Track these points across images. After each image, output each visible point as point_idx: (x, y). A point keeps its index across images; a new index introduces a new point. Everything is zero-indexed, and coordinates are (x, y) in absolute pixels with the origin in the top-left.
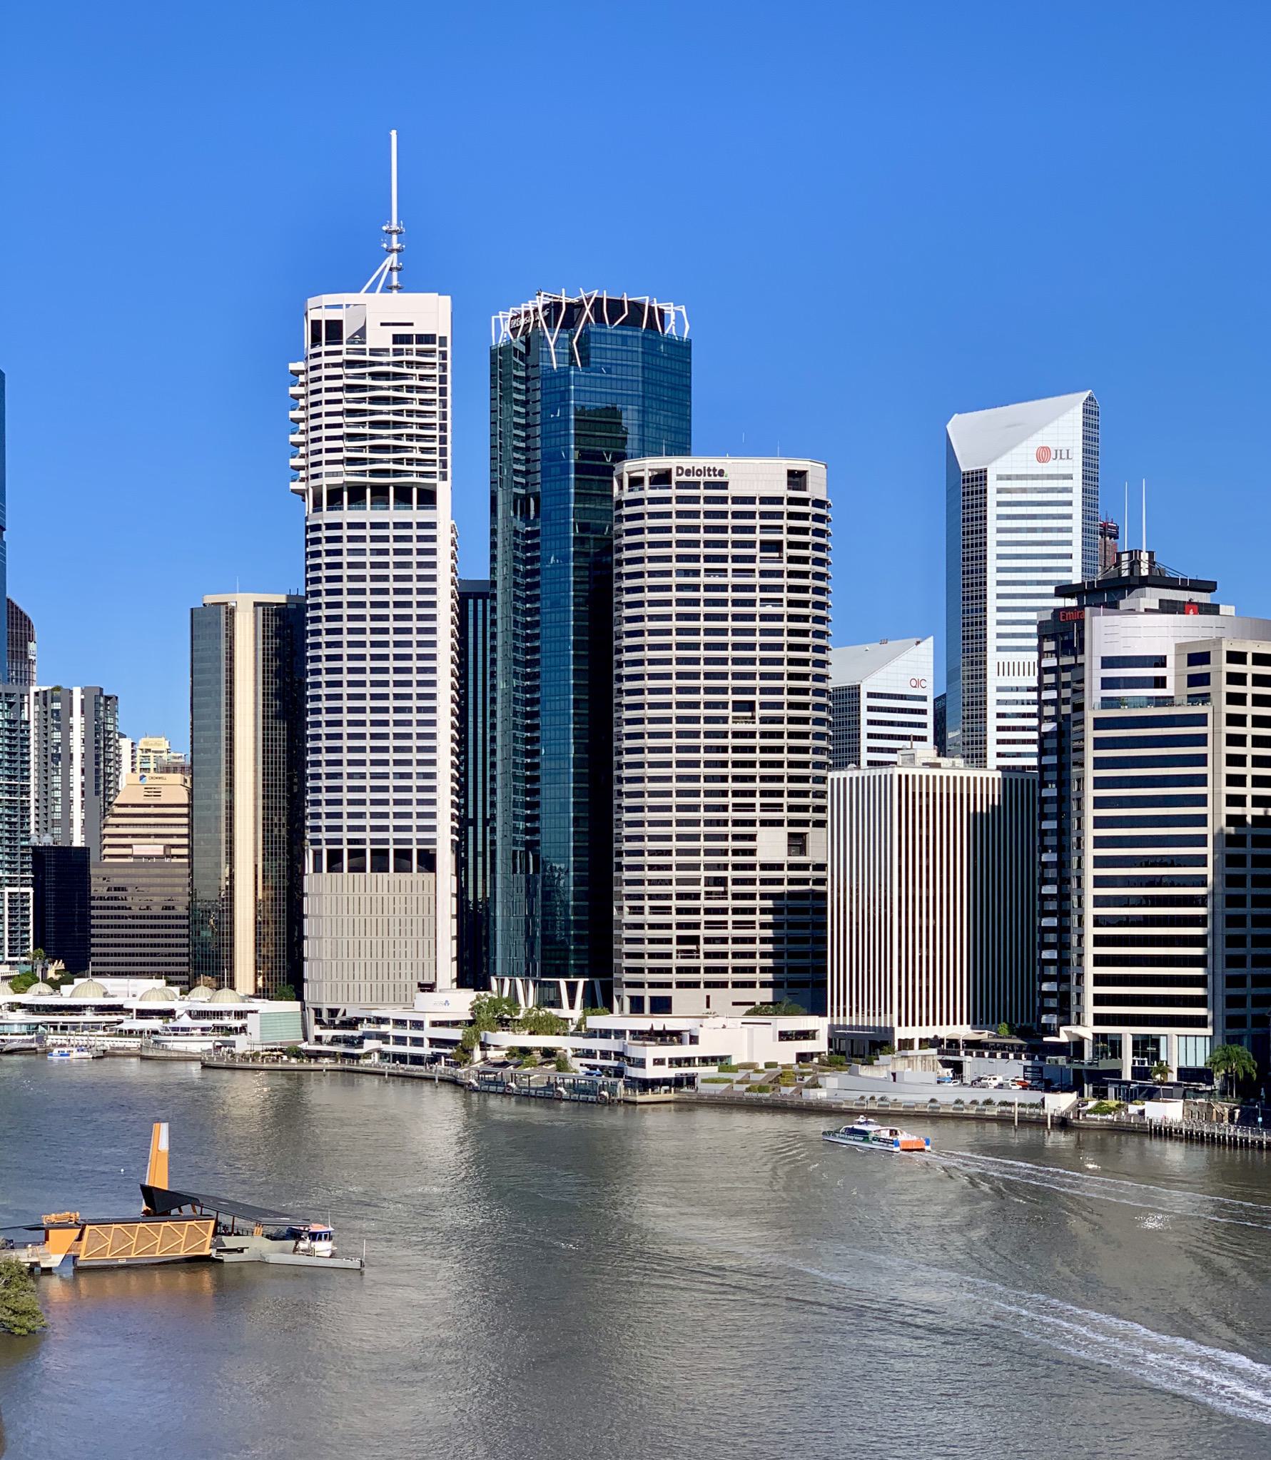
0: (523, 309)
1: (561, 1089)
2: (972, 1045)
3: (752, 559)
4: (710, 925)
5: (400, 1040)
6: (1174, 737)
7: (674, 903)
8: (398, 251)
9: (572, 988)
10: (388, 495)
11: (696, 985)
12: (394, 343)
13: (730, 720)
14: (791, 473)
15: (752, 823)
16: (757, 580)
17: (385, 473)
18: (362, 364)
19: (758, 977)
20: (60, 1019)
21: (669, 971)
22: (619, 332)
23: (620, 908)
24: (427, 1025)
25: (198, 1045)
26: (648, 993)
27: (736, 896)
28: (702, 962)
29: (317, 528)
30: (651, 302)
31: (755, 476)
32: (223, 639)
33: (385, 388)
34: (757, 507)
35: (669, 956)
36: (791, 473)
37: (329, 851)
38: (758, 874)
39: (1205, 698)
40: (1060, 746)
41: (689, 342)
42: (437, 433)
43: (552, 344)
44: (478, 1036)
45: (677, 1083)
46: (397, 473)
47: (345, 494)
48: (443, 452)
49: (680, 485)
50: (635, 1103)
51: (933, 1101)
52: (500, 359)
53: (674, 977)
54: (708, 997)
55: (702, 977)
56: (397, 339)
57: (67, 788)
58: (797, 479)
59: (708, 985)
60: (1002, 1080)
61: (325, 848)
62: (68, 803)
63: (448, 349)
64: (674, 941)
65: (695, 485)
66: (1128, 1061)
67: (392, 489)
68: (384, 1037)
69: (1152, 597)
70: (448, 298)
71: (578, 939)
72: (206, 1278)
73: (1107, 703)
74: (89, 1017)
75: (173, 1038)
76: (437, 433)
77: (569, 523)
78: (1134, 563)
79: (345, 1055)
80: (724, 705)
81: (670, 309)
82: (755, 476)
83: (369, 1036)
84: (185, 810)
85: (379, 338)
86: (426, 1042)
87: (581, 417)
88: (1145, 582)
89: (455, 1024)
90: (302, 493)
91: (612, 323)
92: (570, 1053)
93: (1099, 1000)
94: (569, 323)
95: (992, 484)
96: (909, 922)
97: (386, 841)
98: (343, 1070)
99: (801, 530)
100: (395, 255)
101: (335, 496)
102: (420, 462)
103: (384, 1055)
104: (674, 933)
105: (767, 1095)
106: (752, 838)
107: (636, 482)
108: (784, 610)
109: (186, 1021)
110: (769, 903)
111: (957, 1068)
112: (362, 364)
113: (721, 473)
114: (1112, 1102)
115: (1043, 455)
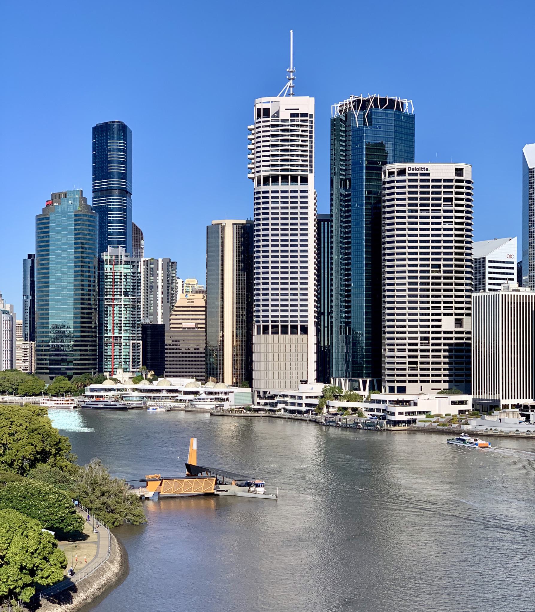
0: (344, 103)
1: (360, 425)
3: (440, 205)
4: (422, 357)
5: (293, 404)
8: (293, 79)
9: (364, 382)
10: (288, 179)
11: (416, 381)
12: (291, 117)
13: (431, 272)
14: (457, 169)
15: (440, 314)
16: (442, 214)
17: (287, 170)
18: (278, 126)
20: (152, 395)
21: (405, 375)
22: (384, 111)
23: (385, 350)
24: (304, 398)
25: (209, 406)
26: (396, 385)
27: (433, 345)
28: (419, 372)
29: (259, 193)
30: (398, 99)
31: (442, 170)
32: (220, 238)
33: (287, 135)
34: (442, 184)
35: (405, 369)
36: (457, 169)
37: (263, 325)
42: (308, 154)
43: (356, 117)
44: (325, 402)
46: (292, 170)
47: (270, 179)
48: (311, 161)
49: (410, 175)
50: (391, 430)
51: (517, 431)
52: (335, 123)
53: (407, 378)
54: (421, 387)
55: (419, 378)
56: (292, 115)
57: (156, 300)
58: (459, 172)
59: (421, 381)
61: (262, 324)
62: (156, 306)
63: (313, 119)
64: (407, 363)
65: (416, 175)
67: (289, 177)
68: (286, 403)
70: (313, 99)
71: (367, 362)
74: (164, 394)
75: (198, 403)
76: (308, 154)
77: (363, 191)
79: (270, 410)
80: (428, 266)
81: (406, 102)
82: (442, 170)
83: (280, 402)
84: (204, 309)
85: (285, 115)
86: (304, 405)
87: (368, 148)
89: (316, 397)
90: (253, 179)
91: (381, 108)
92: (364, 409)
94: (364, 108)
97: (287, 322)
98: (269, 417)
100: (291, 81)
101: (266, 180)
102: (301, 166)
103: (286, 410)
105: (446, 427)
106: (440, 320)
107: (391, 174)
108: (454, 226)
109: (203, 396)
110: (447, 348)
112: (278, 126)
113: (427, 169)
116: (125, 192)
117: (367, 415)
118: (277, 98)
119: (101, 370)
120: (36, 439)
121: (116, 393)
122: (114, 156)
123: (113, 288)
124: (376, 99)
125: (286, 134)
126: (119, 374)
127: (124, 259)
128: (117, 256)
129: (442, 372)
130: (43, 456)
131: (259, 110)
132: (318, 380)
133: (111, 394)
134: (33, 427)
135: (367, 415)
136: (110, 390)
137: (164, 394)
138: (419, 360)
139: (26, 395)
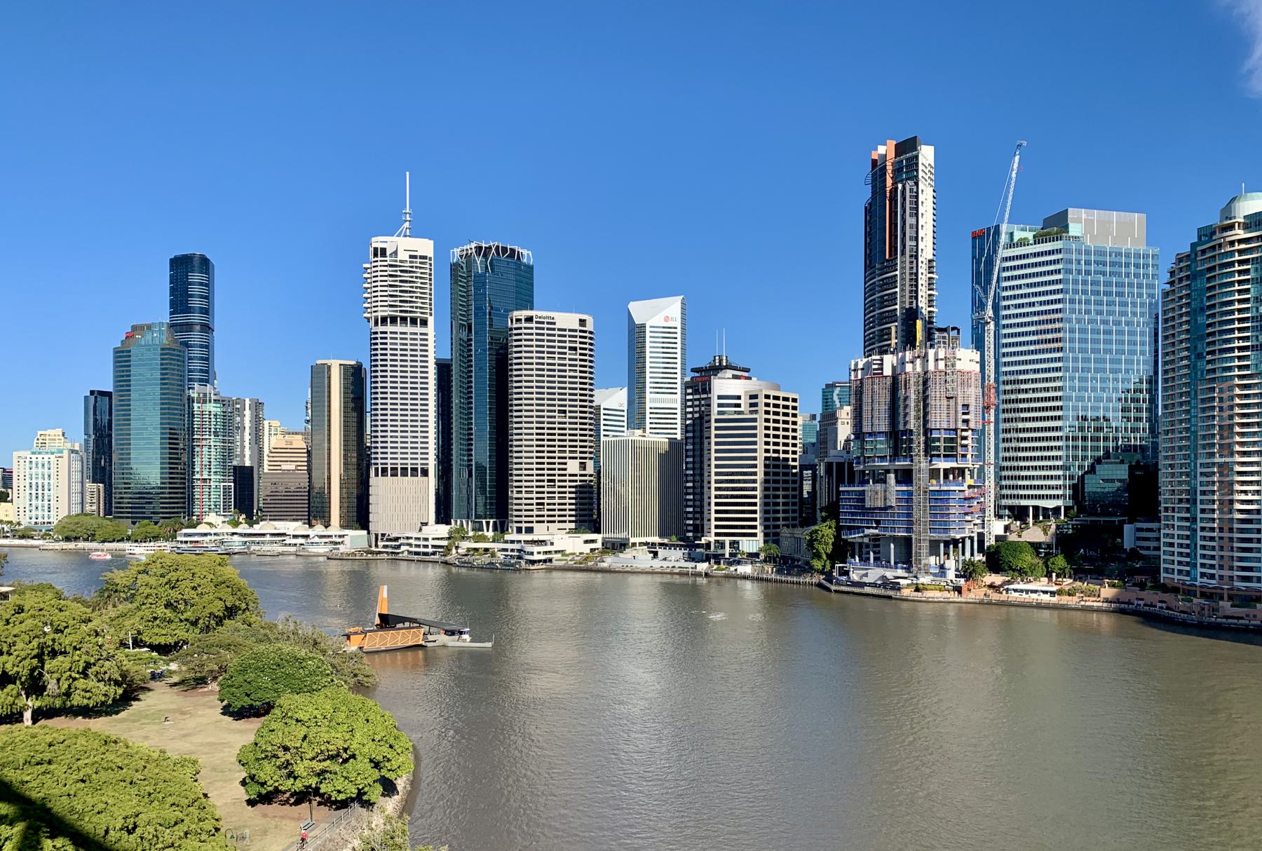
2: (661, 544)
5: (418, 546)
6: (748, 425)
7: (535, 489)
9: (488, 523)
16: (567, 362)
19: (568, 518)
20: (257, 539)
25: (322, 550)
26: (524, 525)
28: (546, 513)
33: (406, 277)
38: (568, 478)
39: (756, 412)
40: (697, 427)
45: (545, 561)
52: (455, 268)
53: (535, 519)
55: (546, 519)
57: (243, 441)
58: (582, 322)
60: (675, 558)
62: (243, 447)
66: (727, 551)
68: (410, 545)
69: (729, 373)
70: (432, 242)
71: (491, 504)
72: (421, 653)
73: (720, 413)
74: (268, 538)
78: (721, 361)
81: (525, 252)
82: (567, 320)
87: (488, 294)
88: (727, 367)
90: (368, 319)
93: (717, 527)
94: (485, 256)
95: (648, 329)
96: (634, 496)
99: (584, 342)
101: (384, 320)
103: (410, 552)
104: (535, 501)
107: (518, 320)
108: (578, 374)
109: (317, 539)
111: (655, 554)
114: (723, 566)
115: (666, 319)
116: (207, 328)
117: (501, 555)
118: (394, 238)
119: (191, 514)
120: (224, 592)
121: (213, 538)
122: (195, 290)
123: (202, 427)
124: (498, 247)
125: (401, 275)
126: (212, 518)
127: (213, 397)
128: (205, 395)
129: (568, 513)
130: (231, 612)
131: (376, 249)
132: (438, 522)
133: (207, 539)
134: (220, 579)
135: (501, 555)
136: (206, 535)
137: (268, 538)
138: (546, 501)
139: (103, 542)
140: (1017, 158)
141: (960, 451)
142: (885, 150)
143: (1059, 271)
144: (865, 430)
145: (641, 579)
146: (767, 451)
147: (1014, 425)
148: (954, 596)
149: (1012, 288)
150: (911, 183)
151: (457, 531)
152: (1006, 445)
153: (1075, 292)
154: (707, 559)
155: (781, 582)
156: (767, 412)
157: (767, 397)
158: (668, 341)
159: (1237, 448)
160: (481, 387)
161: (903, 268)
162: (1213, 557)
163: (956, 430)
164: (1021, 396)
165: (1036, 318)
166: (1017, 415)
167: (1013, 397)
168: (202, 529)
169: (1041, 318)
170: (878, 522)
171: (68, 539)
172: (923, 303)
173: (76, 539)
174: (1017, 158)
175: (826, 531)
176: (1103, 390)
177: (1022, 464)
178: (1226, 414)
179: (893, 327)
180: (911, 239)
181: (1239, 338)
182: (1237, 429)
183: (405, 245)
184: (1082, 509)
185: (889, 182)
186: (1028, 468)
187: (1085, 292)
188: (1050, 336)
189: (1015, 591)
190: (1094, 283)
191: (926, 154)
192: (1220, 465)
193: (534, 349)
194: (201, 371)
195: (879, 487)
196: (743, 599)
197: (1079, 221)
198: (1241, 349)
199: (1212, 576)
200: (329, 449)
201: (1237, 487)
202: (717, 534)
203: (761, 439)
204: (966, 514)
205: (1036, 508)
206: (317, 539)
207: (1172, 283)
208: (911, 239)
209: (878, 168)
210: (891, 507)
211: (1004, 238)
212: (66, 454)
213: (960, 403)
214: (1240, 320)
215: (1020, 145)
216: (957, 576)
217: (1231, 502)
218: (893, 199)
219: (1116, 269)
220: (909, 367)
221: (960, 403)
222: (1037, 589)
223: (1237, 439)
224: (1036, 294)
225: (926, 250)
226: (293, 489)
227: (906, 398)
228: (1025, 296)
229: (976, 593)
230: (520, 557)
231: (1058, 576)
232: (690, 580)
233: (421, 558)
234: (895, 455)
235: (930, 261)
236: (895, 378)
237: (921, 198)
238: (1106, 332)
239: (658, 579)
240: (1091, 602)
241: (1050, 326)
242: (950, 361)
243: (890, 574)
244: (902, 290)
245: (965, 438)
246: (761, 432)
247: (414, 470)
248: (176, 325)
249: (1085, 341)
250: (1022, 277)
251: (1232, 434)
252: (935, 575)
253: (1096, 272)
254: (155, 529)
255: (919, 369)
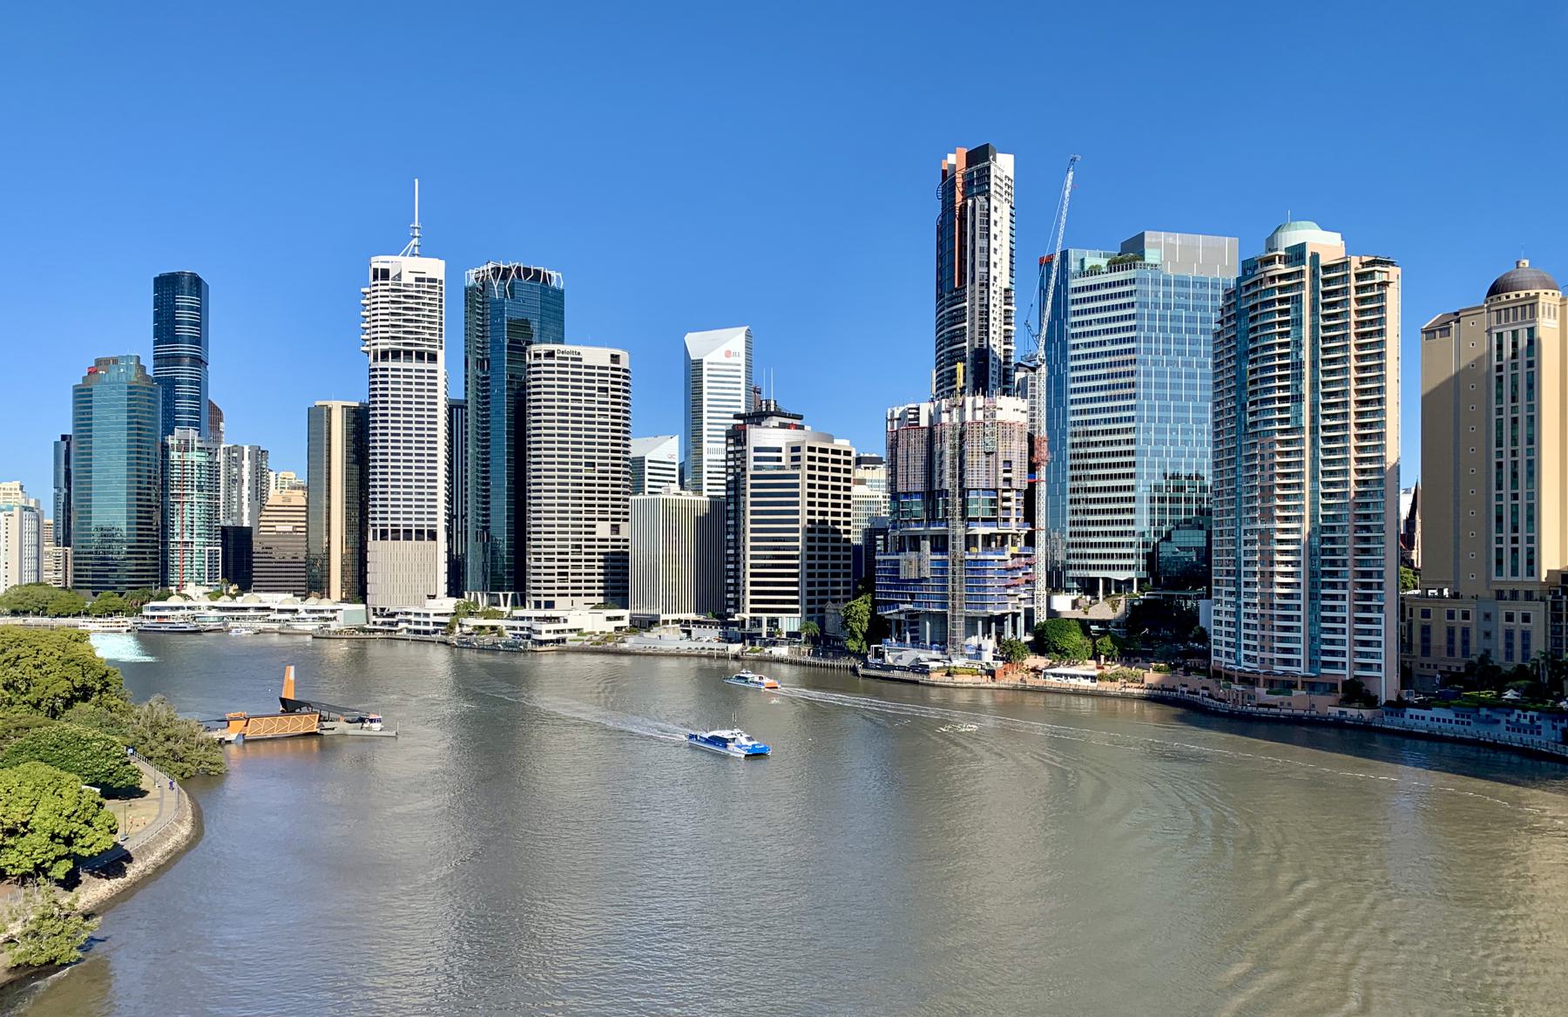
2: (695, 622)
5: (418, 623)
6: (786, 483)
9: (506, 597)
16: (596, 405)
25: (311, 626)
26: (543, 599)
28: (570, 584)
33: (411, 303)
38: (597, 543)
39: (798, 467)
40: (735, 486)
41: (561, 293)
45: (558, 641)
52: (470, 293)
53: (556, 591)
55: (570, 591)
56: (417, 279)
57: (240, 496)
58: (615, 358)
60: (709, 638)
62: (241, 504)
66: (765, 629)
68: (409, 622)
69: (775, 421)
72: (315, 742)
74: (252, 613)
78: (768, 405)
81: (554, 274)
82: (597, 356)
87: (508, 324)
88: (772, 414)
93: (752, 602)
94: (504, 277)
95: (705, 367)
96: (667, 568)
99: (618, 382)
101: (385, 355)
103: (409, 631)
104: (556, 571)
107: (537, 356)
108: (609, 420)
109: (304, 615)
111: (689, 633)
115: (728, 354)
116: (199, 361)
117: (508, 635)
119: (165, 584)
121: (186, 612)
122: (184, 315)
123: (182, 481)
125: (407, 301)
126: (190, 589)
127: (197, 445)
128: (187, 441)
130: (85, 693)
131: (376, 270)
132: (449, 594)
135: (508, 635)
136: (177, 608)
138: (570, 570)
139: (58, 616)
140: (1070, 174)
141: (1001, 515)
142: (955, 159)
143: (1132, 305)
144: (899, 489)
145: (668, 664)
146: (811, 513)
147: (1082, 484)
148: (985, 681)
149: (1082, 324)
150: (982, 199)
151: (466, 606)
152: (1075, 507)
153: (1151, 328)
154: (742, 641)
155: (815, 665)
156: (811, 468)
157: (811, 449)
158: (733, 379)
159: (1278, 513)
160: (499, 432)
161: (973, 298)
162: (1255, 637)
163: (996, 490)
164: (1091, 450)
165: (1107, 360)
166: (1086, 472)
167: (1082, 451)
168: (174, 601)
169: (1113, 359)
170: (912, 596)
171: (15, 613)
172: (996, 343)
173: (25, 613)
174: (1070, 174)
175: (861, 606)
176: (1185, 443)
177: (1091, 529)
178: (1267, 474)
179: (960, 367)
180: (981, 264)
181: (1280, 388)
182: (1278, 491)
183: (409, 266)
184: (1157, 584)
185: (959, 197)
186: (1098, 534)
187: (1163, 329)
188: (1121, 380)
189: (1054, 675)
190: (1190, 319)
191: (1003, 165)
192: (1261, 532)
193: (556, 390)
194: (191, 412)
195: (913, 555)
196: (779, 683)
197: (1157, 245)
198: (1281, 399)
199: (1254, 659)
200: (329, 507)
201: (1278, 557)
202: (753, 610)
203: (803, 499)
204: (1008, 587)
205: (1107, 581)
206: (304, 615)
207: (1221, 322)
208: (981, 264)
209: (948, 178)
210: (925, 579)
211: (1074, 266)
212: (16, 511)
213: (1001, 459)
214: (1281, 367)
215: (1074, 160)
216: (995, 658)
217: (1272, 574)
218: (963, 219)
219: (1201, 302)
220: (945, 418)
221: (1001, 459)
222: (1081, 673)
223: (1278, 502)
224: (1107, 332)
225: (1001, 276)
226: (288, 559)
227: (941, 454)
228: (1097, 333)
229: (1012, 679)
230: (529, 637)
231: (1107, 659)
232: (716, 664)
233: (421, 637)
234: (932, 519)
235: (1006, 290)
236: (931, 429)
237: (994, 216)
238: (1188, 376)
239: (694, 663)
240: (1134, 690)
241: (1122, 369)
242: (991, 412)
243: (923, 656)
244: (972, 324)
245: (1008, 500)
246: (803, 490)
247: (420, 532)
248: (161, 357)
249: (1173, 386)
250: (1093, 311)
251: (1272, 496)
252: (970, 657)
253: (1177, 306)
254: (118, 601)
255: (956, 420)
